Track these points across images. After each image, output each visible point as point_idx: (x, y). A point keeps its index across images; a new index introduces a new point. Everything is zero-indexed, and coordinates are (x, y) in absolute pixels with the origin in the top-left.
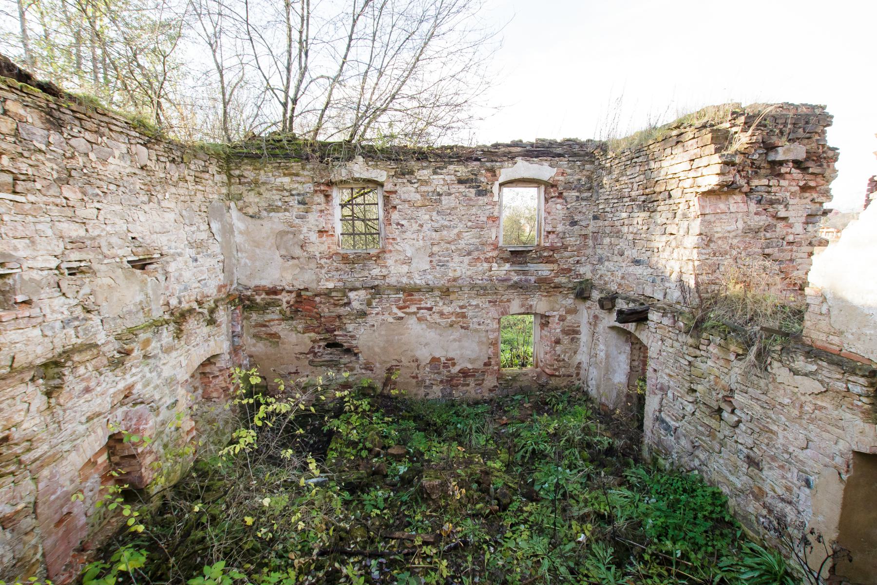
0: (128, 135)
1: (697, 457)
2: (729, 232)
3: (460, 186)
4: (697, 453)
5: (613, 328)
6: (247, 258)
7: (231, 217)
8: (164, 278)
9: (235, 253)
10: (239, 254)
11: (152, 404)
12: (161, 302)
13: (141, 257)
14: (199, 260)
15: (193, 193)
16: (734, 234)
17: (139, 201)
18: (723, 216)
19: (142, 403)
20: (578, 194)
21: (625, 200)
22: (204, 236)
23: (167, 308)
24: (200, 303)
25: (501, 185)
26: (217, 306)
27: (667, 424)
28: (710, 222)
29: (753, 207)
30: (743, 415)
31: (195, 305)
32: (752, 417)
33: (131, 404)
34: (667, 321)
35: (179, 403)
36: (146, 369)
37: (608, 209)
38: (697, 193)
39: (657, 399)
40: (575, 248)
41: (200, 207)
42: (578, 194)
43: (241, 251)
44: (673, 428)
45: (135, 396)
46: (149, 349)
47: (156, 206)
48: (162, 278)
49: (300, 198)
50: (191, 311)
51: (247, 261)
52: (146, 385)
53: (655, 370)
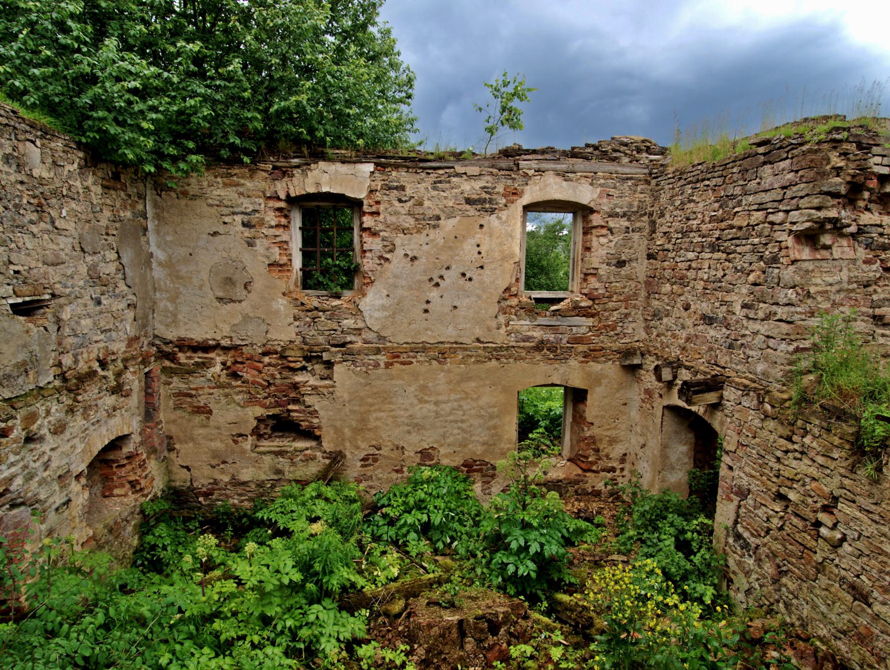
0: (15, 128)
1: (785, 585)
2: (831, 285)
3: (468, 207)
4: (784, 580)
5: (673, 409)
6: (168, 299)
7: (148, 242)
8: (56, 327)
9: (151, 293)
10: (158, 295)
11: (37, 506)
12: (51, 362)
13: (27, 299)
14: (104, 302)
15: (98, 209)
16: (837, 287)
17: (26, 220)
18: (824, 264)
19: (23, 504)
20: (627, 224)
21: (692, 235)
22: (111, 268)
23: (59, 371)
24: (103, 364)
25: (527, 208)
26: (126, 368)
27: (744, 539)
28: (807, 271)
29: (862, 253)
30: (847, 532)
31: (96, 365)
32: (860, 535)
33: (8, 506)
34: (749, 402)
35: (73, 504)
36: (29, 458)
37: (670, 247)
38: (791, 231)
39: (732, 507)
40: (622, 298)
41: (107, 228)
42: (627, 224)
43: (160, 290)
44: (753, 546)
45: (13, 496)
46: (34, 427)
47: (50, 227)
48: (53, 328)
49: (246, 218)
50: (92, 374)
51: (168, 304)
52: (30, 477)
53: (731, 468)
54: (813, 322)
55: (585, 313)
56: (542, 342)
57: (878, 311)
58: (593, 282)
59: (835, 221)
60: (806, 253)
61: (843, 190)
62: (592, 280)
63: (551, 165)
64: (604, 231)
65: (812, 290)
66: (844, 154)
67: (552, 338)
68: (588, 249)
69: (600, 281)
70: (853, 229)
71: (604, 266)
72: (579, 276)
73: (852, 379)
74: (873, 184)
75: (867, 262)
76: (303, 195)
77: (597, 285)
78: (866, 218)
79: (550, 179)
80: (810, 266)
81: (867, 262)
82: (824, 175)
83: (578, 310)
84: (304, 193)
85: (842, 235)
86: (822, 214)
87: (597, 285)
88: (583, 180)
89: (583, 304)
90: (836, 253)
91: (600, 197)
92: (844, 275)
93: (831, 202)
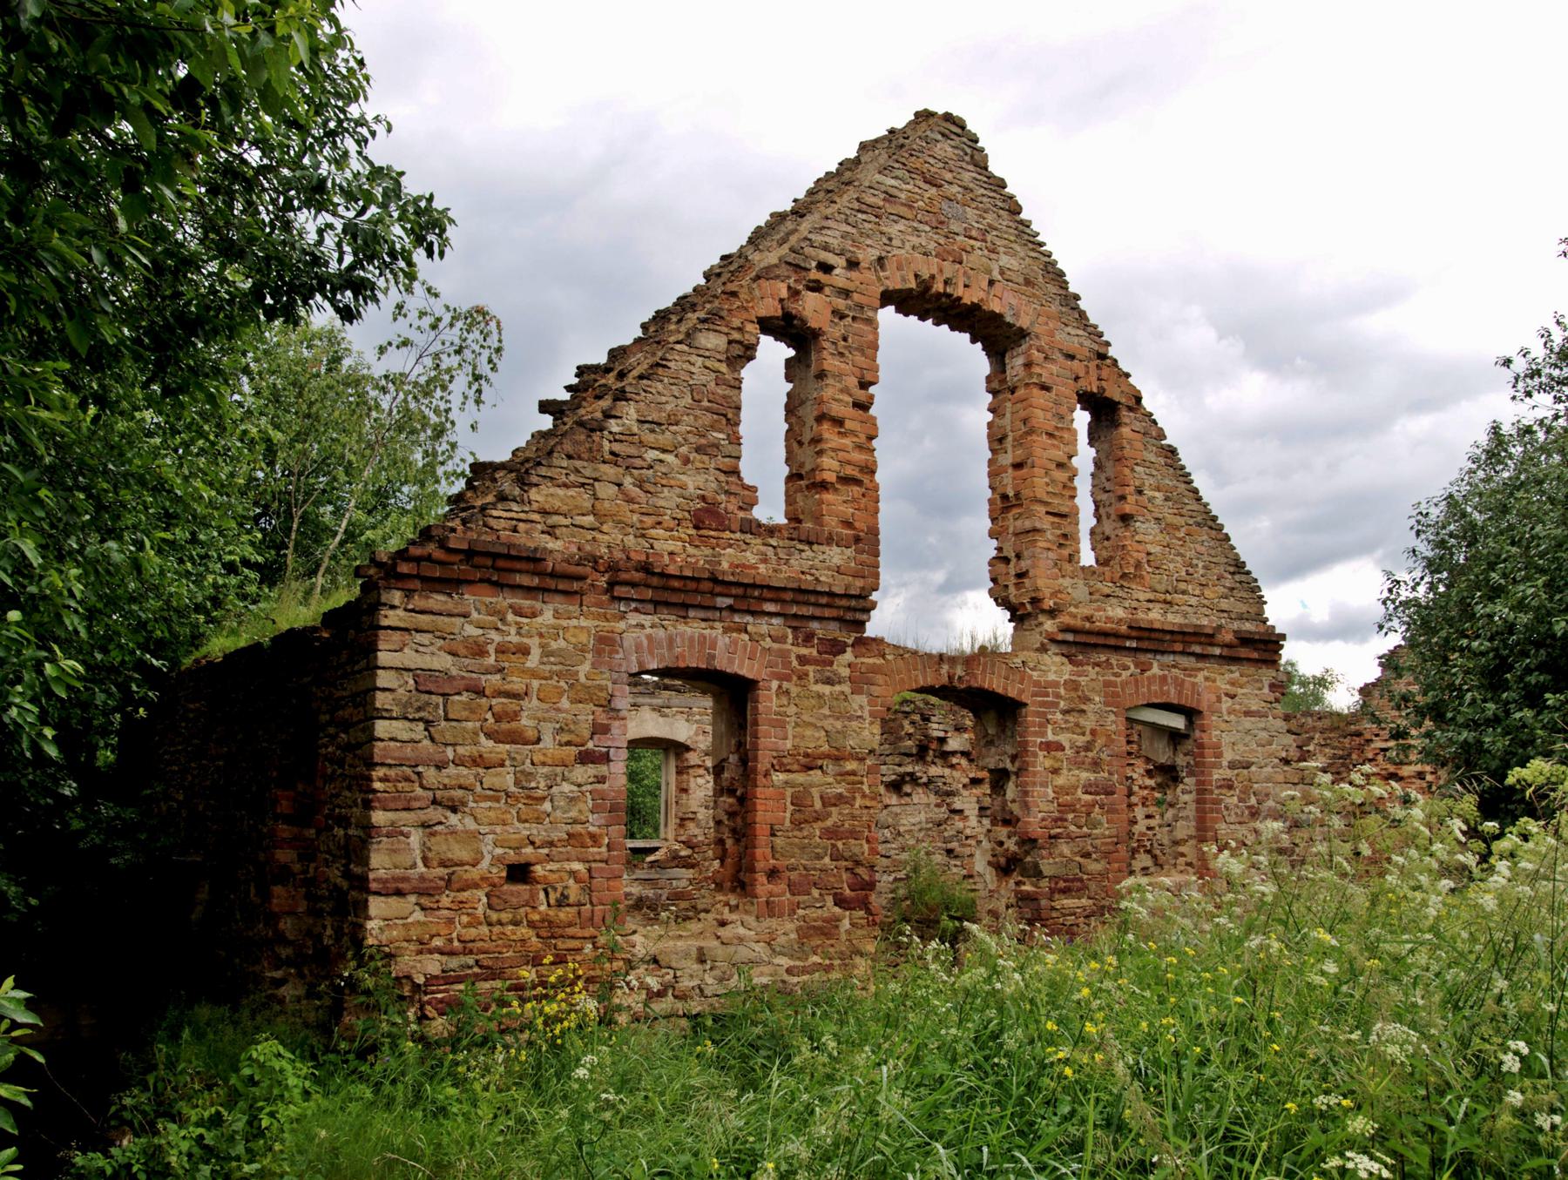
29: (933, 799)
54: (904, 856)
55: (687, 864)
56: (640, 899)
57: (950, 846)
58: (692, 829)
59: (911, 774)
60: (894, 800)
61: (914, 751)
62: (691, 825)
63: (647, 700)
64: (701, 771)
65: (902, 829)
66: (913, 723)
67: (650, 893)
68: (685, 791)
69: (698, 826)
70: (925, 780)
71: (702, 810)
72: (673, 822)
73: (933, 897)
74: (934, 746)
75: (938, 805)
76: (998, 694)
77: (697, 831)
78: (934, 771)
79: (646, 713)
80: (897, 810)
81: (938, 805)
82: (901, 739)
83: (676, 860)
84: (1000, 691)
85: (919, 785)
86: (902, 770)
87: (697, 831)
88: (679, 716)
89: (683, 853)
90: (915, 799)
91: (697, 734)
92: (923, 817)
93: (909, 760)
